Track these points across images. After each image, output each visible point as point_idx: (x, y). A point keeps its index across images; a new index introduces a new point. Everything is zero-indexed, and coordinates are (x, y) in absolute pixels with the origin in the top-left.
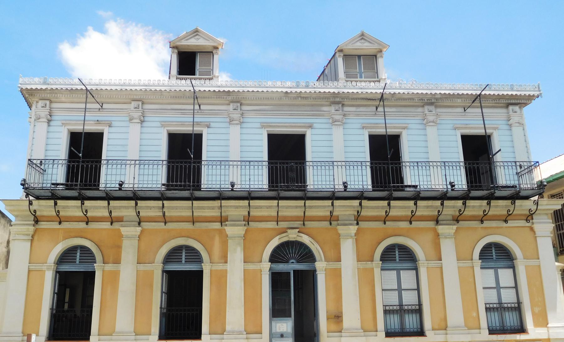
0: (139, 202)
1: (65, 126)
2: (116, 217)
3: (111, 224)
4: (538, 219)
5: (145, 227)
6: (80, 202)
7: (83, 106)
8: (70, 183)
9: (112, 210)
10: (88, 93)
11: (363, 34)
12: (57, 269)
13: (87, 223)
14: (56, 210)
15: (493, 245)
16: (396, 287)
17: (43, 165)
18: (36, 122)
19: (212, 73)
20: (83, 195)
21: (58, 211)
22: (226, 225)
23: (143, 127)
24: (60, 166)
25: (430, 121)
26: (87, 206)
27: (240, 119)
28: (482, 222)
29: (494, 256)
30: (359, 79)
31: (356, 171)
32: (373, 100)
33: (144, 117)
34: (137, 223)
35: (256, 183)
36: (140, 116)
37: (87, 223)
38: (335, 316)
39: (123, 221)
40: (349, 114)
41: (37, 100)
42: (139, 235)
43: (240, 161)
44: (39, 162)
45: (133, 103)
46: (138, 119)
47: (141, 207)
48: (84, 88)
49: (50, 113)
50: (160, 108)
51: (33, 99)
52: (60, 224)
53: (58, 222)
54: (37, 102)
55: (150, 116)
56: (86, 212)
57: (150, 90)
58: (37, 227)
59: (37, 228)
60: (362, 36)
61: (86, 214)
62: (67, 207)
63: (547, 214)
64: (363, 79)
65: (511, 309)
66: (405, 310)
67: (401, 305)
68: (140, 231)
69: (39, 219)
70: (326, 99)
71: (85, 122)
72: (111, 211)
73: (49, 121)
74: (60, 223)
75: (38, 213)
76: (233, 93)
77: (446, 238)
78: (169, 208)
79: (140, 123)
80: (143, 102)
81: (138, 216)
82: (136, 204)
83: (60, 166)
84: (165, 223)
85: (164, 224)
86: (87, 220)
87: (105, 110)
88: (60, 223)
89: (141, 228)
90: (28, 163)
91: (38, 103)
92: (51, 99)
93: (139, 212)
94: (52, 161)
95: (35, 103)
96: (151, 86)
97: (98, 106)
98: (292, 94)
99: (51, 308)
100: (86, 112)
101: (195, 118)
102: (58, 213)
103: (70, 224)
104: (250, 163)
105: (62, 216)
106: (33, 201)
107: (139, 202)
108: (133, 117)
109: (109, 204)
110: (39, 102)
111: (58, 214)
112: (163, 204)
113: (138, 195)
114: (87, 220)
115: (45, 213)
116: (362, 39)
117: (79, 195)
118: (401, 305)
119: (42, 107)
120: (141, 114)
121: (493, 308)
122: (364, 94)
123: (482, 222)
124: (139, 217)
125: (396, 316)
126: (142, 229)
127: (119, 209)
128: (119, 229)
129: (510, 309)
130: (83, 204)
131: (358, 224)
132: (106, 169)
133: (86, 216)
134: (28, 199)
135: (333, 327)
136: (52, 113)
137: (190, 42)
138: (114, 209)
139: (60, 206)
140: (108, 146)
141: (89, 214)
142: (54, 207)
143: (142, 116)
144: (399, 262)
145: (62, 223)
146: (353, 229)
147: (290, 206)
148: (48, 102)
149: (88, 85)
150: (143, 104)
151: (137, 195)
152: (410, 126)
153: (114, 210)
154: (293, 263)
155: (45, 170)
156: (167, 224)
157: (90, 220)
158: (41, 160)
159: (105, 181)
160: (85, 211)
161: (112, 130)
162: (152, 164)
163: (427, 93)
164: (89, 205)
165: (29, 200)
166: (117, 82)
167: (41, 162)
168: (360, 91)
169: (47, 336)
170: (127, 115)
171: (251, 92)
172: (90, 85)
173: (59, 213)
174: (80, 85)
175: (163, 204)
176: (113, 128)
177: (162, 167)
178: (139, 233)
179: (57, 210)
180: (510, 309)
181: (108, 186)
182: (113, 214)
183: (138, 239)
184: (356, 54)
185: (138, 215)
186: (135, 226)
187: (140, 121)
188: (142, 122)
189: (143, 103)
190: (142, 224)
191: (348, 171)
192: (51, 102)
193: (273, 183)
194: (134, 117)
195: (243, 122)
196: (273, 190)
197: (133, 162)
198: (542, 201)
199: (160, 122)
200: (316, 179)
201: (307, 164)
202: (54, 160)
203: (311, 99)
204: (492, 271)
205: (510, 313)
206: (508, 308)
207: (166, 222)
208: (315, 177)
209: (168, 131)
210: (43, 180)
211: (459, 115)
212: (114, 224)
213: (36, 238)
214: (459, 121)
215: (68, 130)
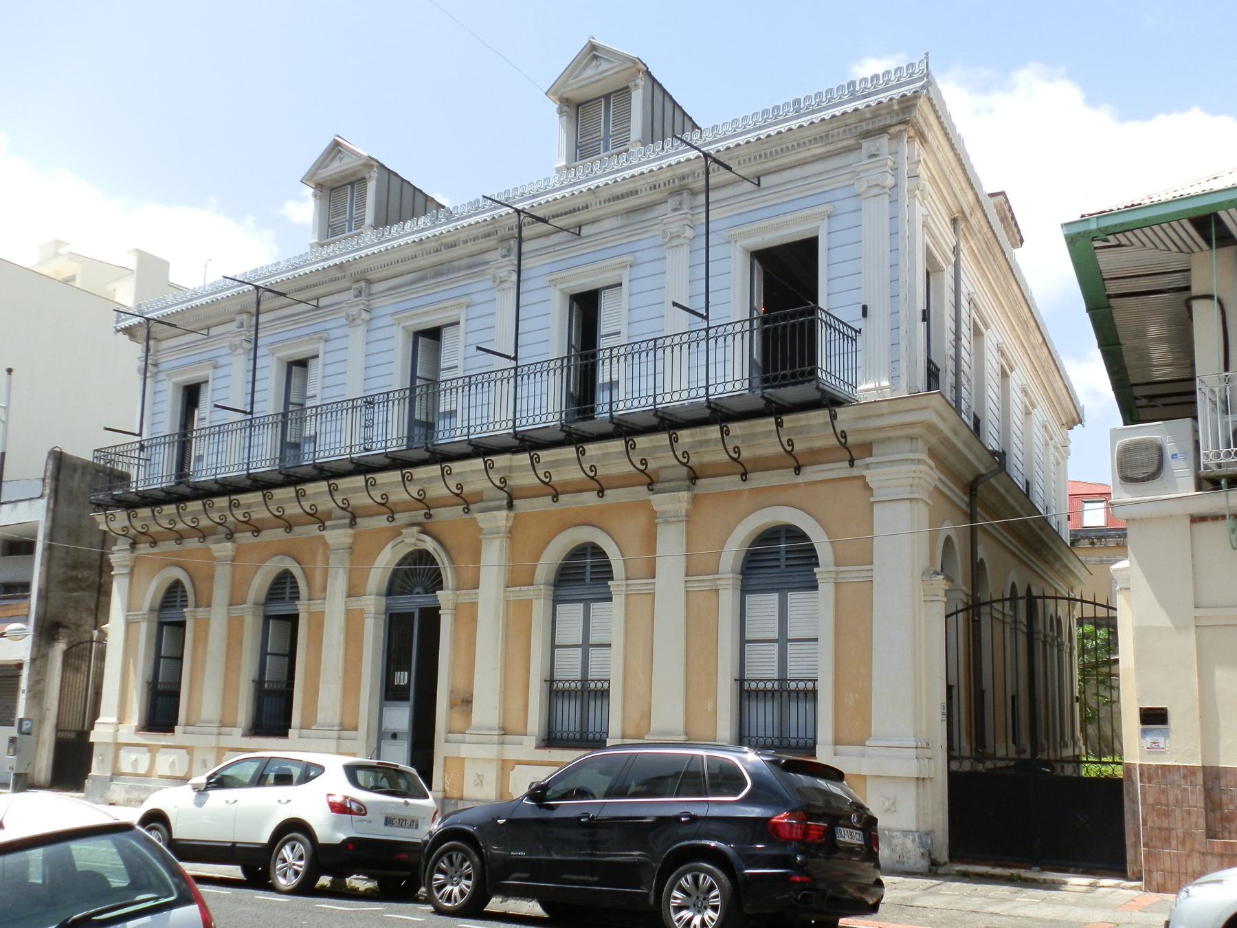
2: (803, 453)
4: (884, 455)
6: (772, 420)
11: (593, 47)
12: (159, 618)
15: (783, 533)
16: (775, 635)
19: (347, 226)
21: (789, 440)
22: (867, 466)
23: (694, 251)
25: (674, 235)
28: (744, 478)
29: (783, 560)
30: (347, 234)
32: (570, 212)
38: (463, 701)
39: (482, 501)
40: (652, 226)
43: (739, 322)
48: (142, 320)
55: (774, 205)
60: (593, 52)
62: (753, 436)
63: (912, 438)
64: (354, 232)
65: (755, 695)
66: (790, 692)
67: (783, 680)
70: (825, 139)
75: (601, 472)
77: (667, 522)
81: (789, 453)
86: (795, 464)
92: (367, 278)
97: (747, 186)
98: (443, 238)
99: (738, 678)
102: (843, 438)
105: (747, 460)
108: (671, 234)
111: (843, 441)
114: (795, 464)
115: (708, 458)
116: (595, 57)
117: (766, 404)
118: (783, 680)
121: (765, 692)
123: (744, 478)
125: (769, 704)
129: (801, 695)
130: (583, 453)
131: (510, 506)
133: (739, 463)
135: (458, 723)
137: (333, 169)
140: (368, 369)
144: (786, 572)
146: (501, 518)
149: (515, 203)
152: (476, 298)
154: (418, 593)
157: (559, 490)
161: (474, 312)
163: (844, 113)
169: (250, 725)
171: (686, 163)
173: (793, 445)
174: (495, 208)
176: (219, 370)
180: (801, 695)
184: (600, 95)
185: (843, 441)
197: (685, 338)
198: (930, 396)
201: (442, 386)
203: (787, 148)
204: (775, 597)
205: (761, 704)
206: (757, 692)
213: (136, 570)
214: (797, 202)
215: (745, 249)
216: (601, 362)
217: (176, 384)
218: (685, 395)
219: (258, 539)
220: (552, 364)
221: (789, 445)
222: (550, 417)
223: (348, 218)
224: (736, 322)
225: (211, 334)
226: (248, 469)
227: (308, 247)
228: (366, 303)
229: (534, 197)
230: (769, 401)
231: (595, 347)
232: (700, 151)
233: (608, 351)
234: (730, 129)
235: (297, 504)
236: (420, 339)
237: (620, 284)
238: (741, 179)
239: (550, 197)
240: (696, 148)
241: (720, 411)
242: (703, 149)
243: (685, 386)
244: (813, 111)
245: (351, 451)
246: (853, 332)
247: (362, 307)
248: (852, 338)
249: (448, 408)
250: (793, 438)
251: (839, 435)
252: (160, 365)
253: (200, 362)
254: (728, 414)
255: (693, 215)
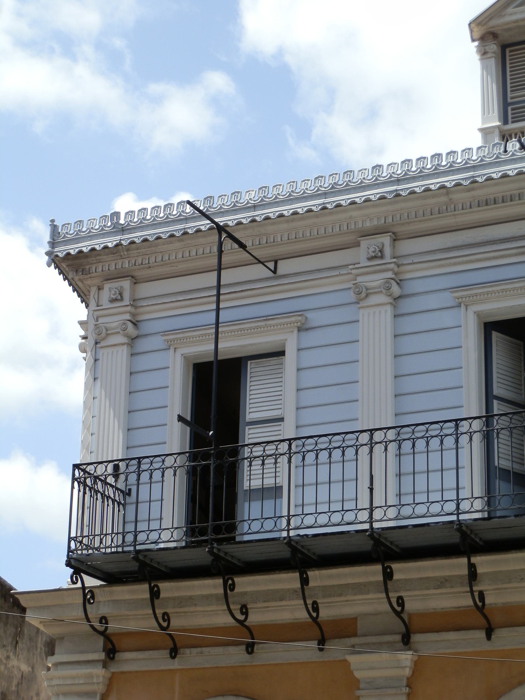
0: (395, 566)
1: (466, 306)
3: (489, 637)
5: (425, 652)
6: (219, 581)
7: (227, 276)
8: (223, 522)
9: (318, 601)
10: (224, 235)
13: (250, 648)
14: (157, 611)
17: (122, 477)
18: (98, 349)
20: (227, 561)
21: (165, 614)
24: (169, 473)
26: (245, 594)
27: (389, 289)
28: (250, 650)
31: (434, 458)
33: (135, 324)
34: (398, 638)
35: (435, 496)
36: (124, 324)
37: (250, 648)
39: (355, 635)
41: (97, 281)
42: (408, 679)
44: (110, 468)
45: (365, 243)
46: (119, 333)
47: (407, 581)
48: (204, 224)
49: (133, 315)
50: (449, 244)
51: (89, 282)
52: (173, 657)
53: (168, 651)
54: (99, 289)
55: (312, 294)
56: (242, 613)
57: (410, 193)
58: (114, 668)
59: (113, 673)
61: (242, 618)
62: (190, 600)
68: (408, 663)
69: (117, 648)
71: (220, 330)
72: (315, 603)
73: (133, 340)
74: (174, 653)
76: (156, 246)
78: (495, 577)
79: (125, 346)
80: (393, 233)
81: (398, 614)
82: (388, 575)
83: (169, 473)
84: (322, 642)
85: (482, 635)
87: (286, 281)
88: (174, 653)
89: (411, 652)
90: (74, 474)
91: (101, 292)
93: (401, 601)
94: (453, 424)
95: (94, 290)
96: (414, 179)
97: (260, 271)
100: (222, 297)
101: (221, 312)
103: (202, 653)
104: (457, 427)
106: (96, 591)
107: (312, 574)
108: (367, 289)
109: (305, 581)
110: (103, 288)
111: (314, 615)
112: (472, 567)
113: (391, 543)
115: (132, 626)
119: (112, 301)
120: (128, 317)
122: (482, 185)
123: (250, 650)
124: (405, 616)
126: (416, 658)
127: (340, 595)
128: (345, 661)
130: (233, 587)
132: (398, 457)
134: (79, 585)
136: (402, 273)
138: (324, 597)
139: (169, 598)
141: (254, 619)
142: (150, 603)
143: (393, 282)
145: (182, 650)
147: (347, 585)
148: (126, 284)
150: (394, 240)
151: (388, 544)
153: (325, 600)
155: (130, 490)
156: (499, 634)
158: (116, 463)
159: (300, 508)
160: (241, 609)
162: (422, 437)
164: (249, 589)
165: (84, 588)
166: (311, 188)
167: (116, 468)
168: (465, 179)
170: (350, 285)
172: (222, 213)
173: (246, 614)
175: (472, 567)
176: (311, 333)
177: (471, 439)
178: (407, 672)
179: (159, 612)
181: (406, 511)
182: (325, 613)
183: (406, 690)
185: (314, 615)
186: (391, 647)
187: (125, 340)
188: (133, 340)
189: (396, 239)
190: (416, 638)
191: (407, 461)
192: (136, 281)
193: (204, 518)
194: (371, 289)
195: (400, 297)
196: (199, 544)
199: (453, 289)
200: (407, 487)
201: (246, 452)
202: (456, 420)
207: (493, 626)
208: (407, 481)
209: (478, 315)
210: (124, 523)
211: (490, 250)
212: (498, 634)
215: (186, 358)
216: (246, 463)
217: (186, 358)
218: (392, 513)
219: (176, 664)
220: (169, 461)
221: (164, 620)
222: (165, 536)
223: (509, 108)
224: (475, 418)
225: (280, 271)
226: (371, 520)
227: (479, 135)
228: (396, 269)
229: (255, 207)
230: (217, 558)
231: (236, 439)
232: (213, 221)
233: (135, 462)
234: (97, 227)
235: (384, 595)
236: (495, 335)
237: (282, 353)
238: (256, 261)
239: (358, 196)
240: (208, 217)
241: (302, 553)
242: (217, 220)
243: (392, 500)
244: (340, 191)
245: (124, 537)
246: (121, 495)
247: (390, 275)
248: (119, 503)
249: (269, 482)
250: (169, 611)
251: (310, 607)
252: (141, 325)
253: (267, 318)
254: (392, 549)
255: (398, 266)
